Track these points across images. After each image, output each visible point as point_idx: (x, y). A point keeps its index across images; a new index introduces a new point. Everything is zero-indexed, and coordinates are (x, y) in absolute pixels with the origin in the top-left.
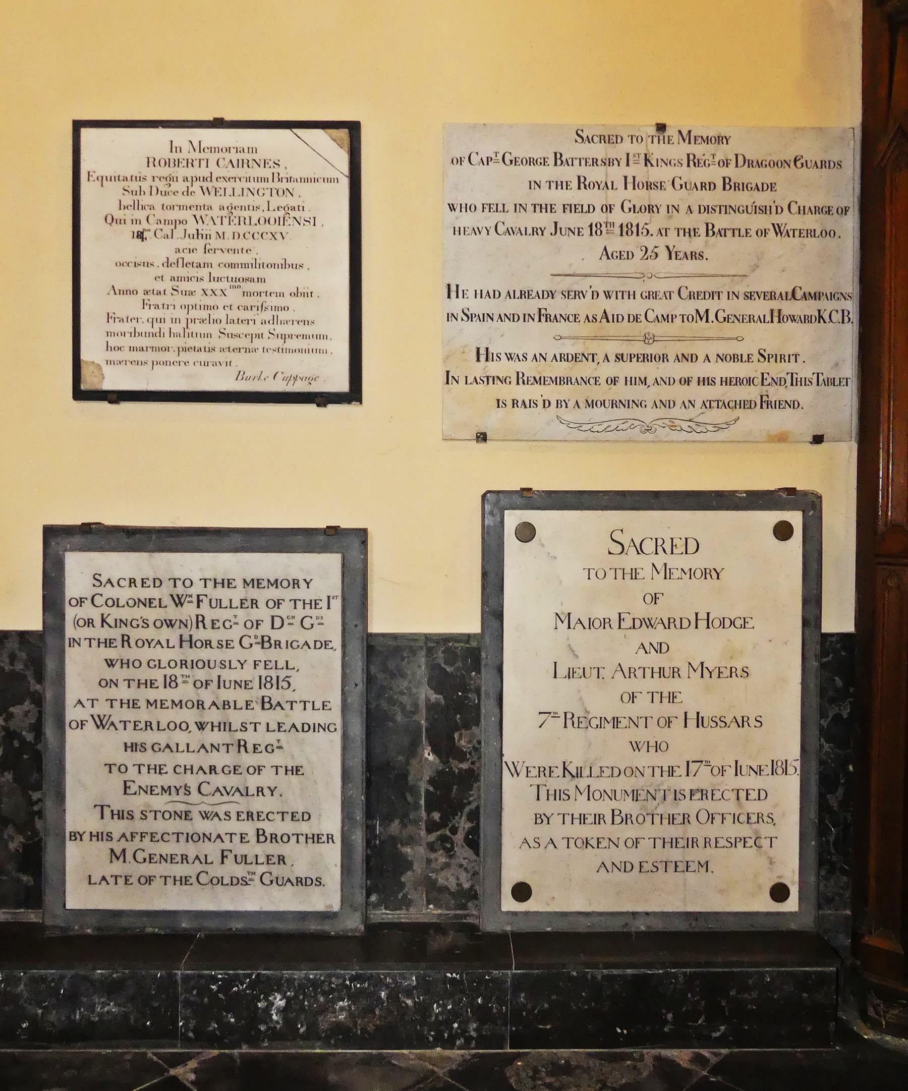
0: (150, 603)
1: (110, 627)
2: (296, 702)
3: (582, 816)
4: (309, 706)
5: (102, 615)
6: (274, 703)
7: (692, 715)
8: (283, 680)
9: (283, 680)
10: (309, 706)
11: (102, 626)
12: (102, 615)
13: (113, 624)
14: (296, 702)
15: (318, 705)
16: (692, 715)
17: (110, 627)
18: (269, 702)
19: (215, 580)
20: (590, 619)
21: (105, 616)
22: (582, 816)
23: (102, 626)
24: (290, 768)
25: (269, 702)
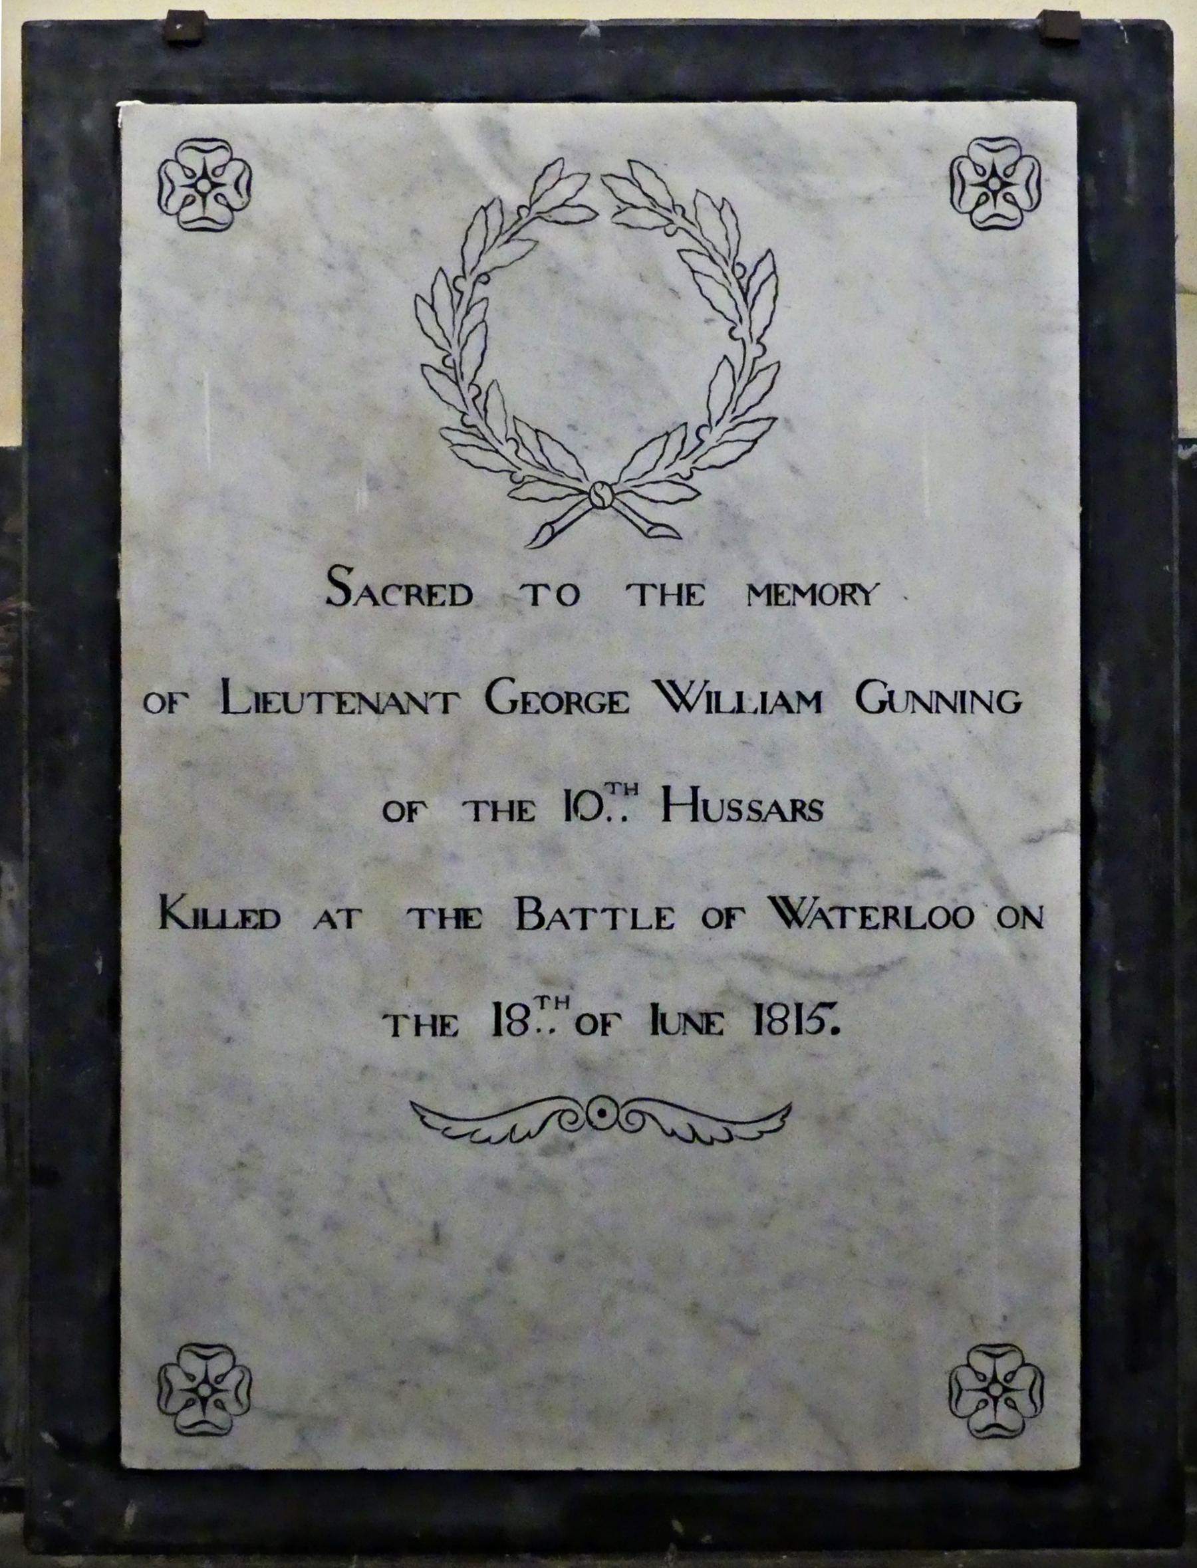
0: (432, 595)
1: (184, 926)
2: (594, 910)
3: (516, 806)
4: (624, 920)
5: (164, 898)
6: (548, 911)
7: (680, 794)
8: (810, 1018)
9: (810, 1018)
10: (624, 920)
11: (164, 926)
12: (164, 898)
13: (189, 921)
14: (594, 910)
15: (646, 917)
16: (680, 794)
17: (184, 926)
18: (536, 912)
19: (495, 804)
20: (568, 792)
21: (170, 902)
22: (516, 806)
23: (164, 926)
24: (429, 1021)
25: (536, 912)
